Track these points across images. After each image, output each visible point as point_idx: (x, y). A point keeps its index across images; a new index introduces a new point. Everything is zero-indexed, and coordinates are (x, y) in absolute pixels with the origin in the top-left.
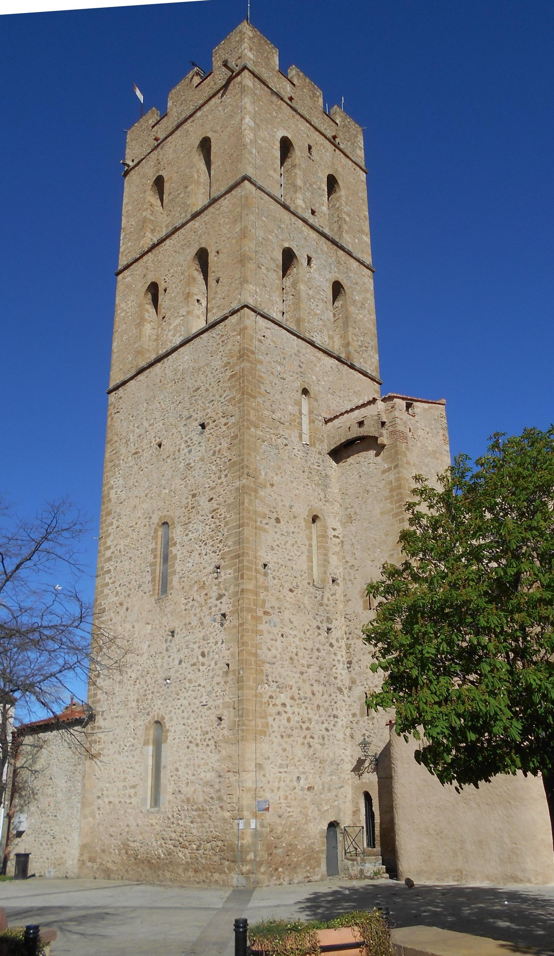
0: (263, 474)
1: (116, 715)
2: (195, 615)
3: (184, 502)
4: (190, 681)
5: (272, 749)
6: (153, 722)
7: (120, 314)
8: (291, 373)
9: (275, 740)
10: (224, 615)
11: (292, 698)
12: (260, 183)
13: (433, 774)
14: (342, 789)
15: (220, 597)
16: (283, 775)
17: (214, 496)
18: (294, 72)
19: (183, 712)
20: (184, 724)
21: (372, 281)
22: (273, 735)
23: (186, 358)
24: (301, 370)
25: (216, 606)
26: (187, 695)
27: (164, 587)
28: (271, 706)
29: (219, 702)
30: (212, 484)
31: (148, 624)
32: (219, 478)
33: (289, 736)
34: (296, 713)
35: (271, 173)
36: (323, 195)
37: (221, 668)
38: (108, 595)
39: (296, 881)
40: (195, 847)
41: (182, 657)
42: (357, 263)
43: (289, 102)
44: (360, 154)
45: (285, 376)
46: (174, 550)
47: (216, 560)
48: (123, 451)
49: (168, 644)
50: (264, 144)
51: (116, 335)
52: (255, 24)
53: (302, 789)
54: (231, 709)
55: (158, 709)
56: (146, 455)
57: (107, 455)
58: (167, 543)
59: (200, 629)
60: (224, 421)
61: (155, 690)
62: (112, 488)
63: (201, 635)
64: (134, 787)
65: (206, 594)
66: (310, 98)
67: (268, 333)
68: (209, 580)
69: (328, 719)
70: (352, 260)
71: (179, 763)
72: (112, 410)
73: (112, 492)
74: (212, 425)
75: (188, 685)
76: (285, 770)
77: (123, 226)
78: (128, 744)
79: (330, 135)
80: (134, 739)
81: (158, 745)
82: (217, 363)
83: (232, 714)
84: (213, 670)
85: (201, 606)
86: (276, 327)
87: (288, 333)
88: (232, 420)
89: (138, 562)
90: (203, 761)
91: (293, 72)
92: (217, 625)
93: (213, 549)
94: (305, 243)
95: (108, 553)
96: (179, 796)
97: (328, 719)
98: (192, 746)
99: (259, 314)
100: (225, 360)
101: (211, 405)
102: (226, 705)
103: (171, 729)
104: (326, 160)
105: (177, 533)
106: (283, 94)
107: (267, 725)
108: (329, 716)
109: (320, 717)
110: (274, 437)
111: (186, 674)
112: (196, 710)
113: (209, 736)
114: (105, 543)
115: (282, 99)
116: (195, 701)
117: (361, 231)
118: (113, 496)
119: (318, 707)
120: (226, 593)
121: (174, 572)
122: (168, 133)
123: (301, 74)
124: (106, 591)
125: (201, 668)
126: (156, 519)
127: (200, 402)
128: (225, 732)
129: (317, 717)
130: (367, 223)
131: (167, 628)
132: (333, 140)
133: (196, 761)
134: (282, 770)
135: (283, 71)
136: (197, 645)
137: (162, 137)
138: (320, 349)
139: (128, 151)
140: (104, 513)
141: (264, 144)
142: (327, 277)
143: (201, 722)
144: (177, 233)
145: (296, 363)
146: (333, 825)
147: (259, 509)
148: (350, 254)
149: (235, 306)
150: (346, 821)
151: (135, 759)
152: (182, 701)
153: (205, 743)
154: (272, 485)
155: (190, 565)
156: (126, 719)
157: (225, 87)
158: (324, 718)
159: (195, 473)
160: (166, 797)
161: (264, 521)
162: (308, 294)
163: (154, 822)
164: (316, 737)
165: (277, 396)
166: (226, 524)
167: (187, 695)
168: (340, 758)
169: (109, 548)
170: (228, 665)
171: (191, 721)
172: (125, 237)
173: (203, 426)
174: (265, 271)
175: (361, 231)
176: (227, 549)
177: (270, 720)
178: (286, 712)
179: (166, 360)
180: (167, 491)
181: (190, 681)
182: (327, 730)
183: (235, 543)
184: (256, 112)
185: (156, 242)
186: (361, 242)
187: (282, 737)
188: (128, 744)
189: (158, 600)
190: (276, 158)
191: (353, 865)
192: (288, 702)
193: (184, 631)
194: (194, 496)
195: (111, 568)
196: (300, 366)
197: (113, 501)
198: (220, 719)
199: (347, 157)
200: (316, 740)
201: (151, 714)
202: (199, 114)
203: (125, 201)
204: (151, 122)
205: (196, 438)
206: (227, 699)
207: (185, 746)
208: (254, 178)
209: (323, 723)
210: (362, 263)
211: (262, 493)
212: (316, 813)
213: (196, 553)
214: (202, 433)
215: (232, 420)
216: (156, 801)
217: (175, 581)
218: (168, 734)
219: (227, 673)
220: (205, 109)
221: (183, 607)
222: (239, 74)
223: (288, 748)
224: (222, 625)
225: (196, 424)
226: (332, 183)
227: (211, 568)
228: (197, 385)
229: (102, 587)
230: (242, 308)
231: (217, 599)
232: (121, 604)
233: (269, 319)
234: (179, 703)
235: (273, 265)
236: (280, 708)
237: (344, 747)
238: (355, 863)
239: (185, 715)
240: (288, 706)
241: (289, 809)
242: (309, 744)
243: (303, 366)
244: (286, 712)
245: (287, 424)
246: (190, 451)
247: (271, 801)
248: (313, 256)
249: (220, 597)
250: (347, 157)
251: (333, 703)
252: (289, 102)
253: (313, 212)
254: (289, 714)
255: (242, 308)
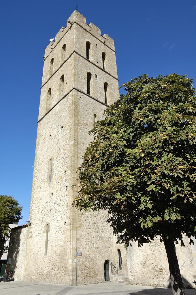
0: (80, 140)
1: (36, 223)
2: (59, 187)
3: (57, 151)
4: (57, 210)
5: (83, 233)
6: (46, 225)
7: (41, 99)
8: (90, 109)
9: (84, 230)
10: (67, 186)
11: (91, 215)
12: (79, 53)
13: (130, 244)
14: (110, 248)
15: (66, 180)
16: (87, 243)
17: (65, 148)
18: (91, 24)
19: (55, 221)
20: (55, 225)
21: (118, 83)
22: (83, 228)
23: (58, 108)
24: (94, 108)
25: (65, 183)
26: (56, 215)
27: (50, 179)
28: (83, 217)
29: (65, 217)
30: (64, 145)
31: (46, 192)
32: (66, 142)
33: (90, 228)
34: (92, 220)
35: (83, 51)
36: (101, 58)
37: (66, 205)
38: (35, 184)
39: (92, 283)
40: (57, 270)
41: (55, 202)
42: (113, 78)
43: (89, 32)
44: (113, 47)
45: (88, 110)
46: (53, 167)
47: (65, 168)
48: (41, 139)
49: (51, 198)
50: (81, 43)
51: (40, 106)
52: (78, 11)
53: (95, 248)
54: (69, 219)
55: (48, 220)
56: (47, 139)
57: (37, 141)
58: (52, 165)
59: (60, 192)
60: (68, 124)
61: (47, 214)
62: (38, 151)
63: (60, 194)
64: (40, 248)
65: (62, 180)
66: (96, 31)
67: (82, 97)
68: (63, 175)
69: (104, 222)
70: (111, 77)
71: (53, 239)
72: (38, 127)
73: (38, 152)
74: (65, 126)
75: (56, 211)
76: (88, 241)
77: (43, 75)
78: (39, 233)
79: (103, 41)
80: (41, 231)
81: (47, 232)
82: (66, 107)
83: (69, 221)
84: (64, 205)
85: (61, 184)
86: (85, 95)
87: (89, 98)
88: (70, 124)
89: (44, 172)
90: (60, 238)
91: (91, 24)
92: (65, 190)
93: (64, 165)
94: (94, 71)
95: (36, 171)
96: (52, 251)
97: (104, 222)
98: (57, 232)
99: (79, 91)
100: (68, 106)
101: (64, 120)
102: (67, 218)
103: (51, 227)
104: (102, 48)
105: (54, 162)
106: (87, 30)
107: (81, 224)
108: (105, 221)
109: (101, 221)
110: (84, 129)
111: (56, 207)
112: (58, 220)
113: (62, 229)
114: (35, 168)
115: (87, 31)
116: (58, 217)
117: (114, 69)
118: (38, 153)
119: (101, 218)
120: (68, 179)
121: (53, 174)
122: (55, 46)
123: (93, 25)
124: (35, 183)
125: (60, 205)
126: (49, 159)
127: (61, 120)
128: (67, 227)
129: (100, 221)
130: (116, 66)
131: (51, 193)
132: (104, 43)
133: (58, 238)
134: (87, 241)
135: (88, 24)
136: (59, 197)
137: (53, 48)
138: (100, 102)
139: (45, 54)
140: (35, 159)
141: (81, 43)
142: (102, 81)
143: (60, 224)
144: (57, 72)
145: (92, 106)
146: (107, 262)
147: (79, 151)
148: (110, 75)
149: (71, 89)
150: (111, 261)
151: (41, 238)
152: (55, 217)
153: (61, 232)
154: (83, 144)
155: (58, 171)
156: (39, 224)
157: (71, 28)
158: (103, 222)
159: (60, 142)
160: (49, 251)
161: (80, 155)
162: (96, 86)
163: (45, 260)
164: (100, 229)
165: (85, 116)
166: (68, 156)
167: (56, 215)
168: (109, 237)
169: (36, 169)
170: (68, 203)
171: (57, 224)
172: (43, 78)
173: (62, 127)
174: (81, 78)
175: (114, 69)
176: (68, 165)
177: (82, 223)
178: (88, 220)
179: (52, 109)
180: (52, 149)
181: (57, 210)
182: (104, 226)
183: (70, 162)
184: (78, 34)
185: (51, 76)
186: (115, 72)
187: (87, 229)
188: (39, 233)
189: (49, 184)
190: (85, 47)
191: (114, 277)
192: (89, 216)
193: (56, 193)
194: (59, 149)
195: (37, 175)
196: (93, 107)
197: (38, 154)
198: (65, 222)
199: (109, 47)
200: (100, 230)
201: (46, 222)
202: (63, 39)
203: (44, 68)
204: (51, 45)
205: (60, 131)
206: (67, 215)
207: (55, 233)
208: (77, 52)
209: (102, 224)
210: (114, 78)
211: (80, 146)
212: (100, 257)
213: (59, 167)
214: (62, 129)
215: (70, 124)
216: (46, 253)
217: (53, 177)
218: (50, 229)
219: (67, 206)
220: (64, 37)
221: (56, 185)
222: (73, 24)
223: (89, 233)
224: (66, 190)
225: (60, 127)
226: (104, 55)
227: (64, 171)
228: (61, 115)
229: (34, 181)
230: (73, 89)
231: (65, 181)
232: (39, 186)
233: (82, 93)
234: (53, 217)
235: (84, 77)
236: (86, 218)
237: (111, 233)
238: (115, 276)
239: (55, 222)
240: (89, 218)
241: (90, 255)
242: (97, 231)
243: (94, 107)
244: (88, 220)
245: (89, 125)
246: (59, 136)
247: (82, 252)
248: (98, 75)
249: (66, 180)
250: (109, 47)
251: (106, 217)
252: (89, 32)
253: (97, 62)
254: (90, 221)
255: (73, 89)
